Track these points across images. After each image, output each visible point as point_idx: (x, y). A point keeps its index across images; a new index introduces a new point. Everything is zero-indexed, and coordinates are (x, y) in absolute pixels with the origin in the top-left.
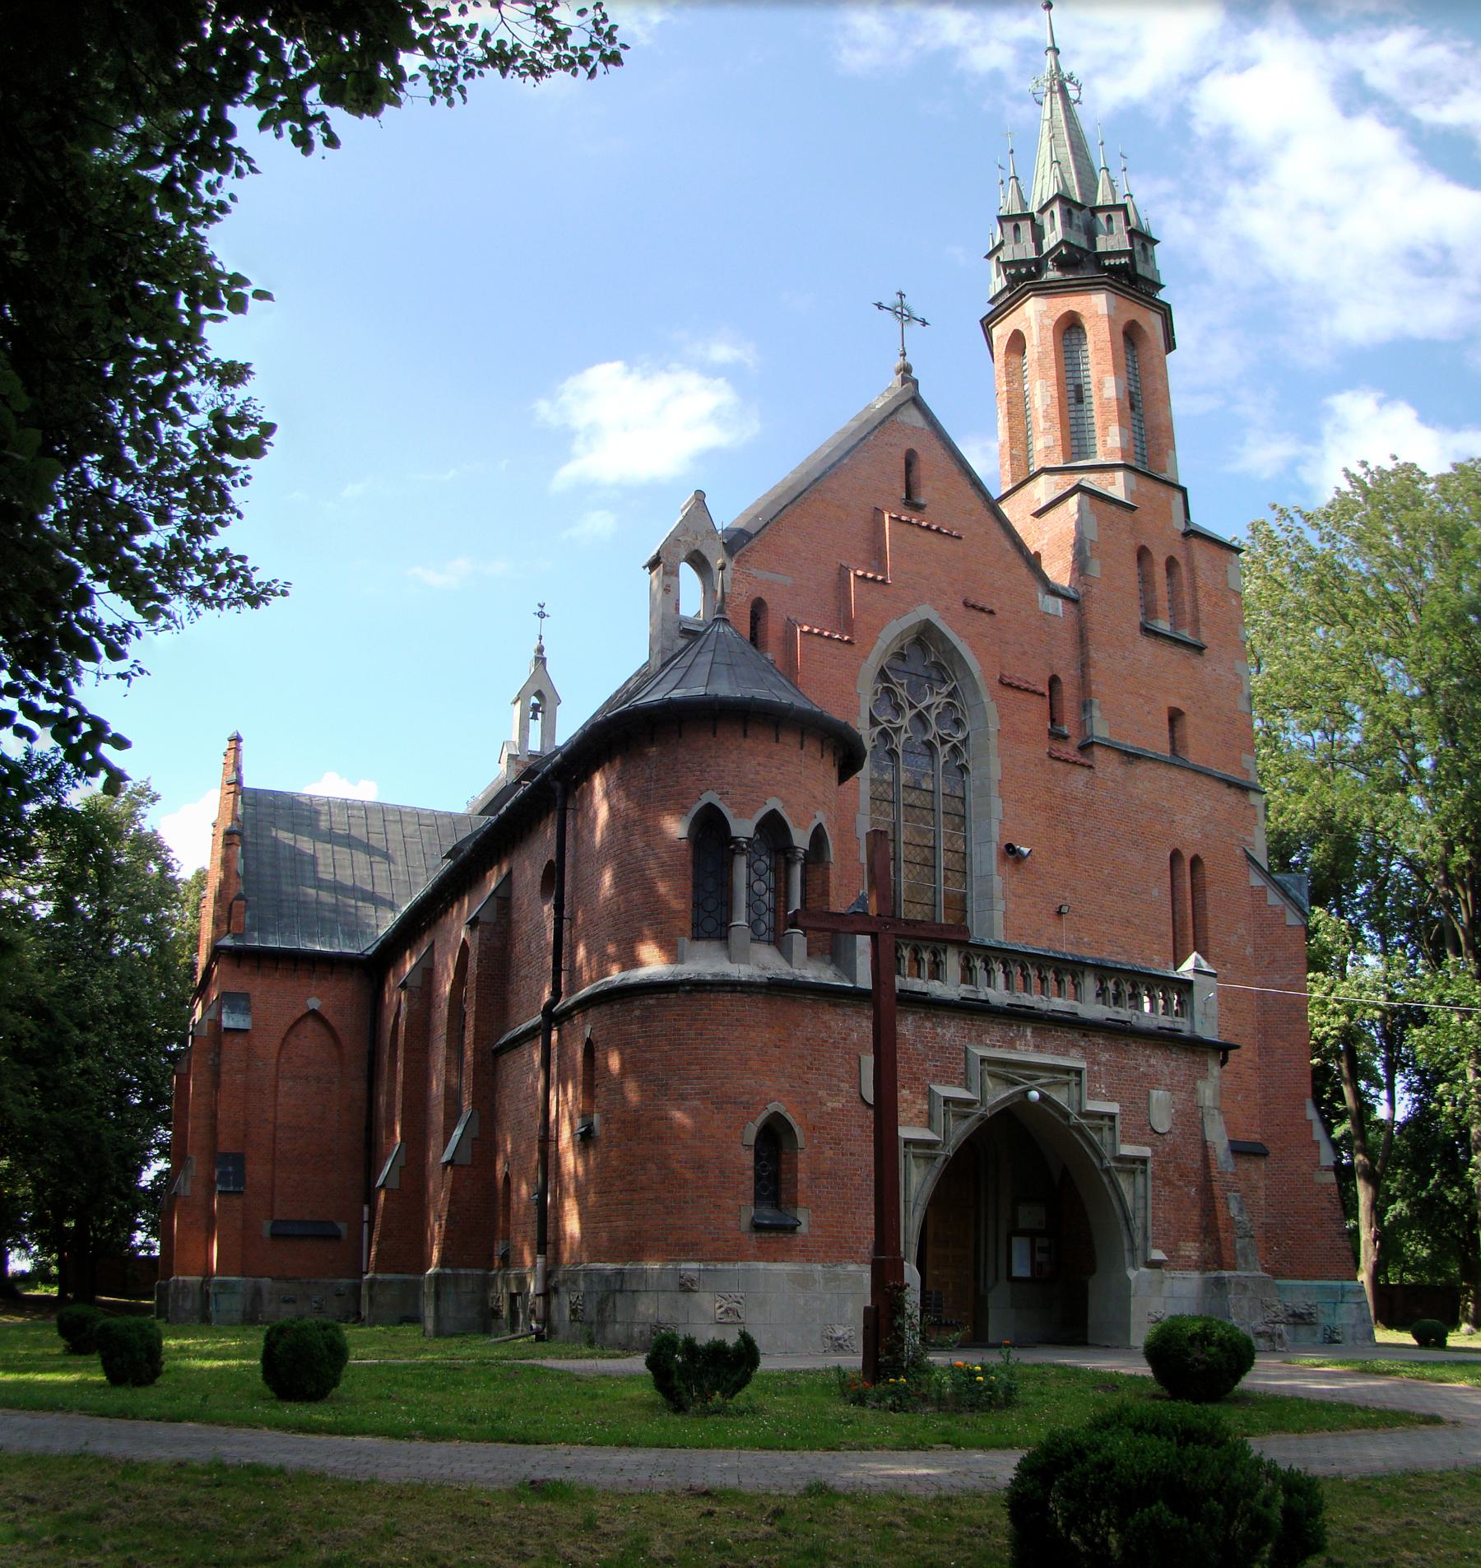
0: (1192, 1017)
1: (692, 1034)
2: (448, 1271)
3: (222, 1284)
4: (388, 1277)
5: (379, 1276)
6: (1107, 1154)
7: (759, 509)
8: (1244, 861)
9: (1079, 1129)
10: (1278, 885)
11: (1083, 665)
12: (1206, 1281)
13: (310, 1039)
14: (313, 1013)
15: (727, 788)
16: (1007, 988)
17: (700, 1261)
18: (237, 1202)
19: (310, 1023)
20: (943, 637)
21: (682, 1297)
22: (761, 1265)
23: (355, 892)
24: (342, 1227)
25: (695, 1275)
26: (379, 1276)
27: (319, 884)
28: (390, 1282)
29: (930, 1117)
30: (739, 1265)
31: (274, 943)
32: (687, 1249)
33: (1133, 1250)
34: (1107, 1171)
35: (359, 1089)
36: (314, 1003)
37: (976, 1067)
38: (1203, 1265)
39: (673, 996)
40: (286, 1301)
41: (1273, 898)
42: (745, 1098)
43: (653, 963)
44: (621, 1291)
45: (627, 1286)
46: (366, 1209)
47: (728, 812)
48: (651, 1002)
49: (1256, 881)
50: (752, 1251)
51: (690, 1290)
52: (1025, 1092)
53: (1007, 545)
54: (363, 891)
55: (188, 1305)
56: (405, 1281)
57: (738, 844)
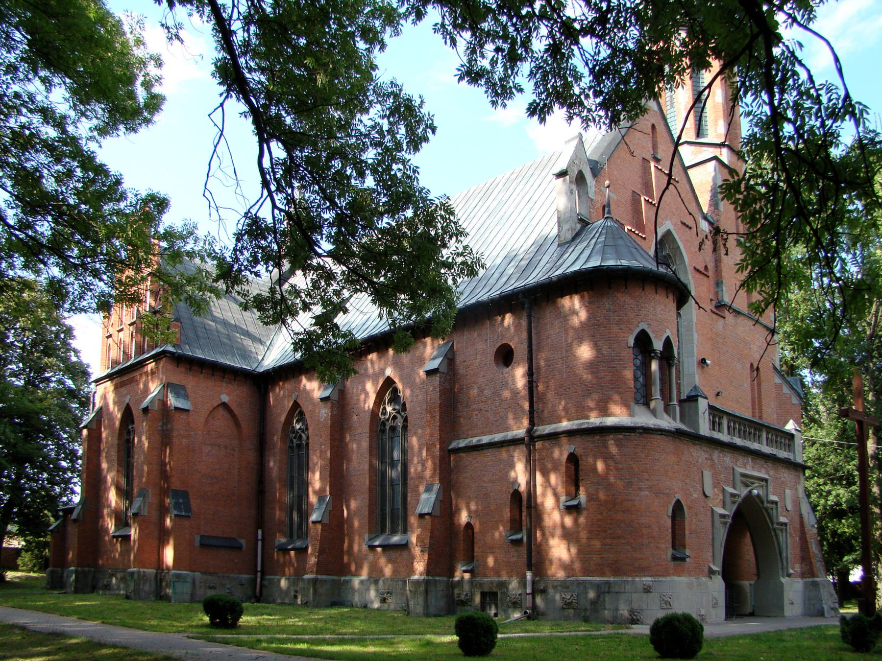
0: (794, 452)
1: (643, 456)
2: (431, 578)
3: (178, 576)
4: (324, 577)
5: (319, 577)
6: (775, 520)
7: (601, 150)
8: (772, 370)
9: (766, 509)
10: (788, 383)
11: (716, 261)
12: (806, 584)
13: (221, 421)
14: (224, 405)
15: (651, 322)
16: (729, 434)
17: (651, 576)
18: (186, 523)
19: (221, 411)
20: (674, 240)
21: (645, 596)
22: (676, 578)
23: (236, 328)
24: (243, 542)
25: (651, 584)
26: (319, 577)
27: (214, 319)
28: (325, 581)
29: (724, 502)
30: (668, 578)
31: (200, 354)
32: (643, 570)
33: (782, 569)
34: (774, 530)
35: (251, 456)
36: (225, 398)
37: (738, 478)
38: (803, 575)
39: (632, 434)
40: (210, 588)
41: (786, 390)
42: (667, 491)
43: (618, 416)
44: (609, 592)
45: (613, 590)
46: (260, 532)
47: (652, 336)
48: (621, 437)
49: (778, 380)
50: (672, 571)
51: (649, 592)
52: (750, 492)
53: (688, 187)
54: (241, 328)
55: (147, 588)
56: (334, 580)
57: (656, 354)
